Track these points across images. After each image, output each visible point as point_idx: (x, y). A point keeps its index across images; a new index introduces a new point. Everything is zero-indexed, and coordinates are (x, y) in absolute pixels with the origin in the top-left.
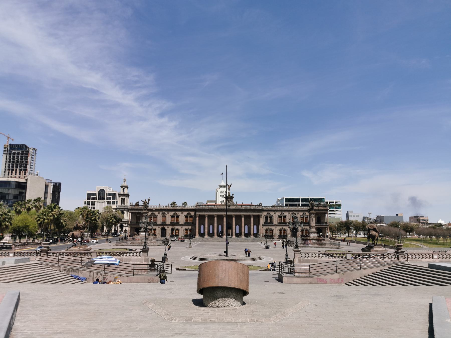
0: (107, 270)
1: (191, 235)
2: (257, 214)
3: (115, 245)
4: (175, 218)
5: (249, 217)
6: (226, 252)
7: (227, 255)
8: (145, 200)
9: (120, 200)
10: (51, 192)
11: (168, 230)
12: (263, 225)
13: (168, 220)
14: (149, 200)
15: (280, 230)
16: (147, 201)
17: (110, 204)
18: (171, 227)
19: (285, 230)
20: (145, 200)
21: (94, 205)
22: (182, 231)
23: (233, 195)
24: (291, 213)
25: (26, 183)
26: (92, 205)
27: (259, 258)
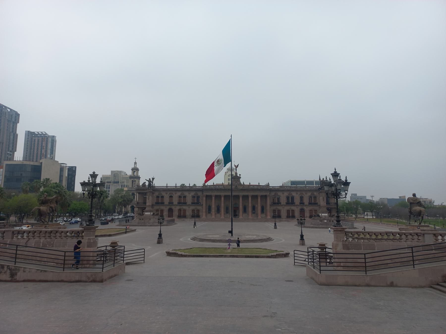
0: (20, 256)
1: (196, 215)
2: (264, 194)
3: (118, 226)
4: (182, 199)
5: (256, 197)
6: (231, 232)
7: (232, 235)
8: (150, 179)
9: (131, 182)
10: (66, 175)
11: (176, 209)
12: (270, 205)
13: (175, 200)
14: (153, 179)
16: (151, 180)
17: (124, 187)
18: (178, 208)
20: (150, 179)
21: (109, 188)
22: (189, 211)
23: (240, 175)
24: (299, 193)
25: (41, 166)
26: (107, 188)
27: (269, 239)
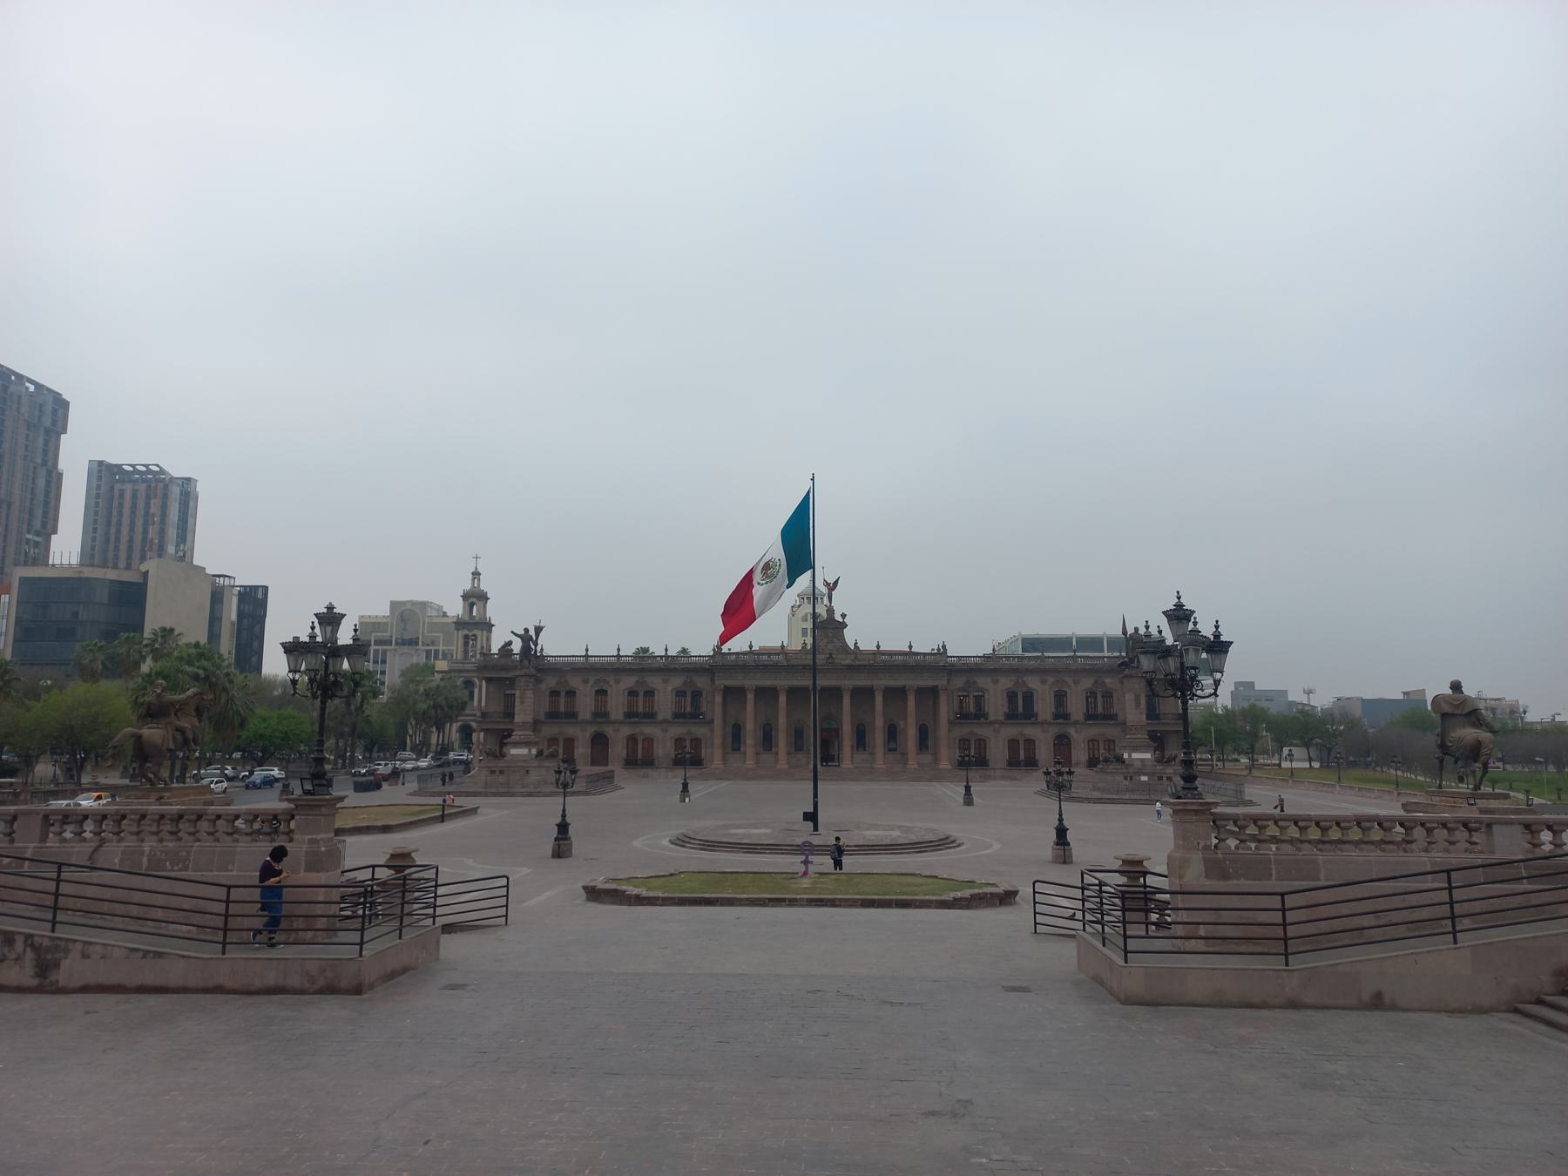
1: (689, 759)
2: (930, 683)
3: (413, 794)
4: (641, 699)
5: (901, 693)
6: (811, 817)
7: (816, 828)
8: (526, 630)
9: (461, 642)
10: (234, 617)
11: (618, 737)
12: (950, 722)
13: (617, 705)
14: (538, 630)
15: (679, 741)
16: (532, 633)
17: (436, 658)
18: (626, 731)
19: (649, 741)
20: (526, 630)
21: (384, 662)
22: (664, 742)
23: (843, 616)
24: (1051, 680)
25: (145, 584)
26: (375, 662)
